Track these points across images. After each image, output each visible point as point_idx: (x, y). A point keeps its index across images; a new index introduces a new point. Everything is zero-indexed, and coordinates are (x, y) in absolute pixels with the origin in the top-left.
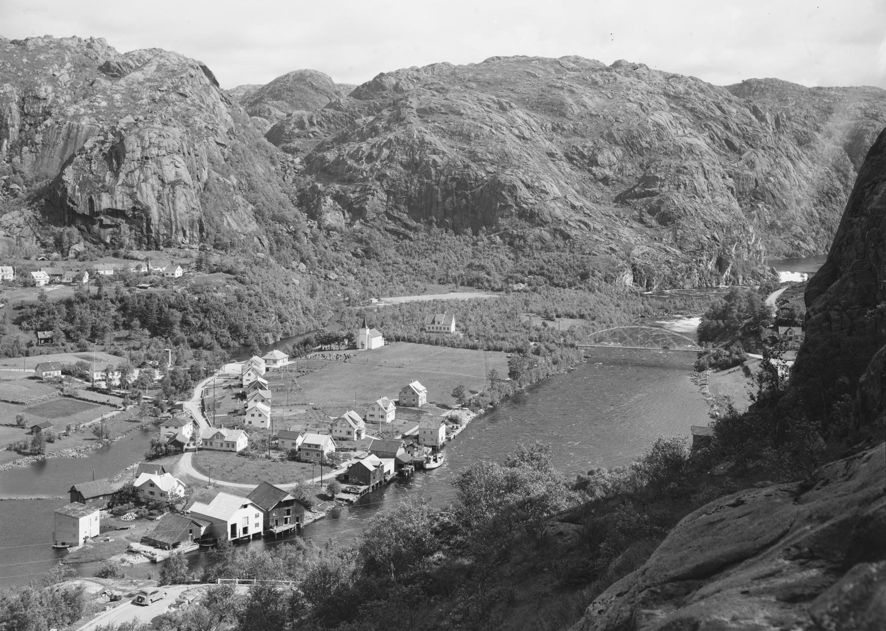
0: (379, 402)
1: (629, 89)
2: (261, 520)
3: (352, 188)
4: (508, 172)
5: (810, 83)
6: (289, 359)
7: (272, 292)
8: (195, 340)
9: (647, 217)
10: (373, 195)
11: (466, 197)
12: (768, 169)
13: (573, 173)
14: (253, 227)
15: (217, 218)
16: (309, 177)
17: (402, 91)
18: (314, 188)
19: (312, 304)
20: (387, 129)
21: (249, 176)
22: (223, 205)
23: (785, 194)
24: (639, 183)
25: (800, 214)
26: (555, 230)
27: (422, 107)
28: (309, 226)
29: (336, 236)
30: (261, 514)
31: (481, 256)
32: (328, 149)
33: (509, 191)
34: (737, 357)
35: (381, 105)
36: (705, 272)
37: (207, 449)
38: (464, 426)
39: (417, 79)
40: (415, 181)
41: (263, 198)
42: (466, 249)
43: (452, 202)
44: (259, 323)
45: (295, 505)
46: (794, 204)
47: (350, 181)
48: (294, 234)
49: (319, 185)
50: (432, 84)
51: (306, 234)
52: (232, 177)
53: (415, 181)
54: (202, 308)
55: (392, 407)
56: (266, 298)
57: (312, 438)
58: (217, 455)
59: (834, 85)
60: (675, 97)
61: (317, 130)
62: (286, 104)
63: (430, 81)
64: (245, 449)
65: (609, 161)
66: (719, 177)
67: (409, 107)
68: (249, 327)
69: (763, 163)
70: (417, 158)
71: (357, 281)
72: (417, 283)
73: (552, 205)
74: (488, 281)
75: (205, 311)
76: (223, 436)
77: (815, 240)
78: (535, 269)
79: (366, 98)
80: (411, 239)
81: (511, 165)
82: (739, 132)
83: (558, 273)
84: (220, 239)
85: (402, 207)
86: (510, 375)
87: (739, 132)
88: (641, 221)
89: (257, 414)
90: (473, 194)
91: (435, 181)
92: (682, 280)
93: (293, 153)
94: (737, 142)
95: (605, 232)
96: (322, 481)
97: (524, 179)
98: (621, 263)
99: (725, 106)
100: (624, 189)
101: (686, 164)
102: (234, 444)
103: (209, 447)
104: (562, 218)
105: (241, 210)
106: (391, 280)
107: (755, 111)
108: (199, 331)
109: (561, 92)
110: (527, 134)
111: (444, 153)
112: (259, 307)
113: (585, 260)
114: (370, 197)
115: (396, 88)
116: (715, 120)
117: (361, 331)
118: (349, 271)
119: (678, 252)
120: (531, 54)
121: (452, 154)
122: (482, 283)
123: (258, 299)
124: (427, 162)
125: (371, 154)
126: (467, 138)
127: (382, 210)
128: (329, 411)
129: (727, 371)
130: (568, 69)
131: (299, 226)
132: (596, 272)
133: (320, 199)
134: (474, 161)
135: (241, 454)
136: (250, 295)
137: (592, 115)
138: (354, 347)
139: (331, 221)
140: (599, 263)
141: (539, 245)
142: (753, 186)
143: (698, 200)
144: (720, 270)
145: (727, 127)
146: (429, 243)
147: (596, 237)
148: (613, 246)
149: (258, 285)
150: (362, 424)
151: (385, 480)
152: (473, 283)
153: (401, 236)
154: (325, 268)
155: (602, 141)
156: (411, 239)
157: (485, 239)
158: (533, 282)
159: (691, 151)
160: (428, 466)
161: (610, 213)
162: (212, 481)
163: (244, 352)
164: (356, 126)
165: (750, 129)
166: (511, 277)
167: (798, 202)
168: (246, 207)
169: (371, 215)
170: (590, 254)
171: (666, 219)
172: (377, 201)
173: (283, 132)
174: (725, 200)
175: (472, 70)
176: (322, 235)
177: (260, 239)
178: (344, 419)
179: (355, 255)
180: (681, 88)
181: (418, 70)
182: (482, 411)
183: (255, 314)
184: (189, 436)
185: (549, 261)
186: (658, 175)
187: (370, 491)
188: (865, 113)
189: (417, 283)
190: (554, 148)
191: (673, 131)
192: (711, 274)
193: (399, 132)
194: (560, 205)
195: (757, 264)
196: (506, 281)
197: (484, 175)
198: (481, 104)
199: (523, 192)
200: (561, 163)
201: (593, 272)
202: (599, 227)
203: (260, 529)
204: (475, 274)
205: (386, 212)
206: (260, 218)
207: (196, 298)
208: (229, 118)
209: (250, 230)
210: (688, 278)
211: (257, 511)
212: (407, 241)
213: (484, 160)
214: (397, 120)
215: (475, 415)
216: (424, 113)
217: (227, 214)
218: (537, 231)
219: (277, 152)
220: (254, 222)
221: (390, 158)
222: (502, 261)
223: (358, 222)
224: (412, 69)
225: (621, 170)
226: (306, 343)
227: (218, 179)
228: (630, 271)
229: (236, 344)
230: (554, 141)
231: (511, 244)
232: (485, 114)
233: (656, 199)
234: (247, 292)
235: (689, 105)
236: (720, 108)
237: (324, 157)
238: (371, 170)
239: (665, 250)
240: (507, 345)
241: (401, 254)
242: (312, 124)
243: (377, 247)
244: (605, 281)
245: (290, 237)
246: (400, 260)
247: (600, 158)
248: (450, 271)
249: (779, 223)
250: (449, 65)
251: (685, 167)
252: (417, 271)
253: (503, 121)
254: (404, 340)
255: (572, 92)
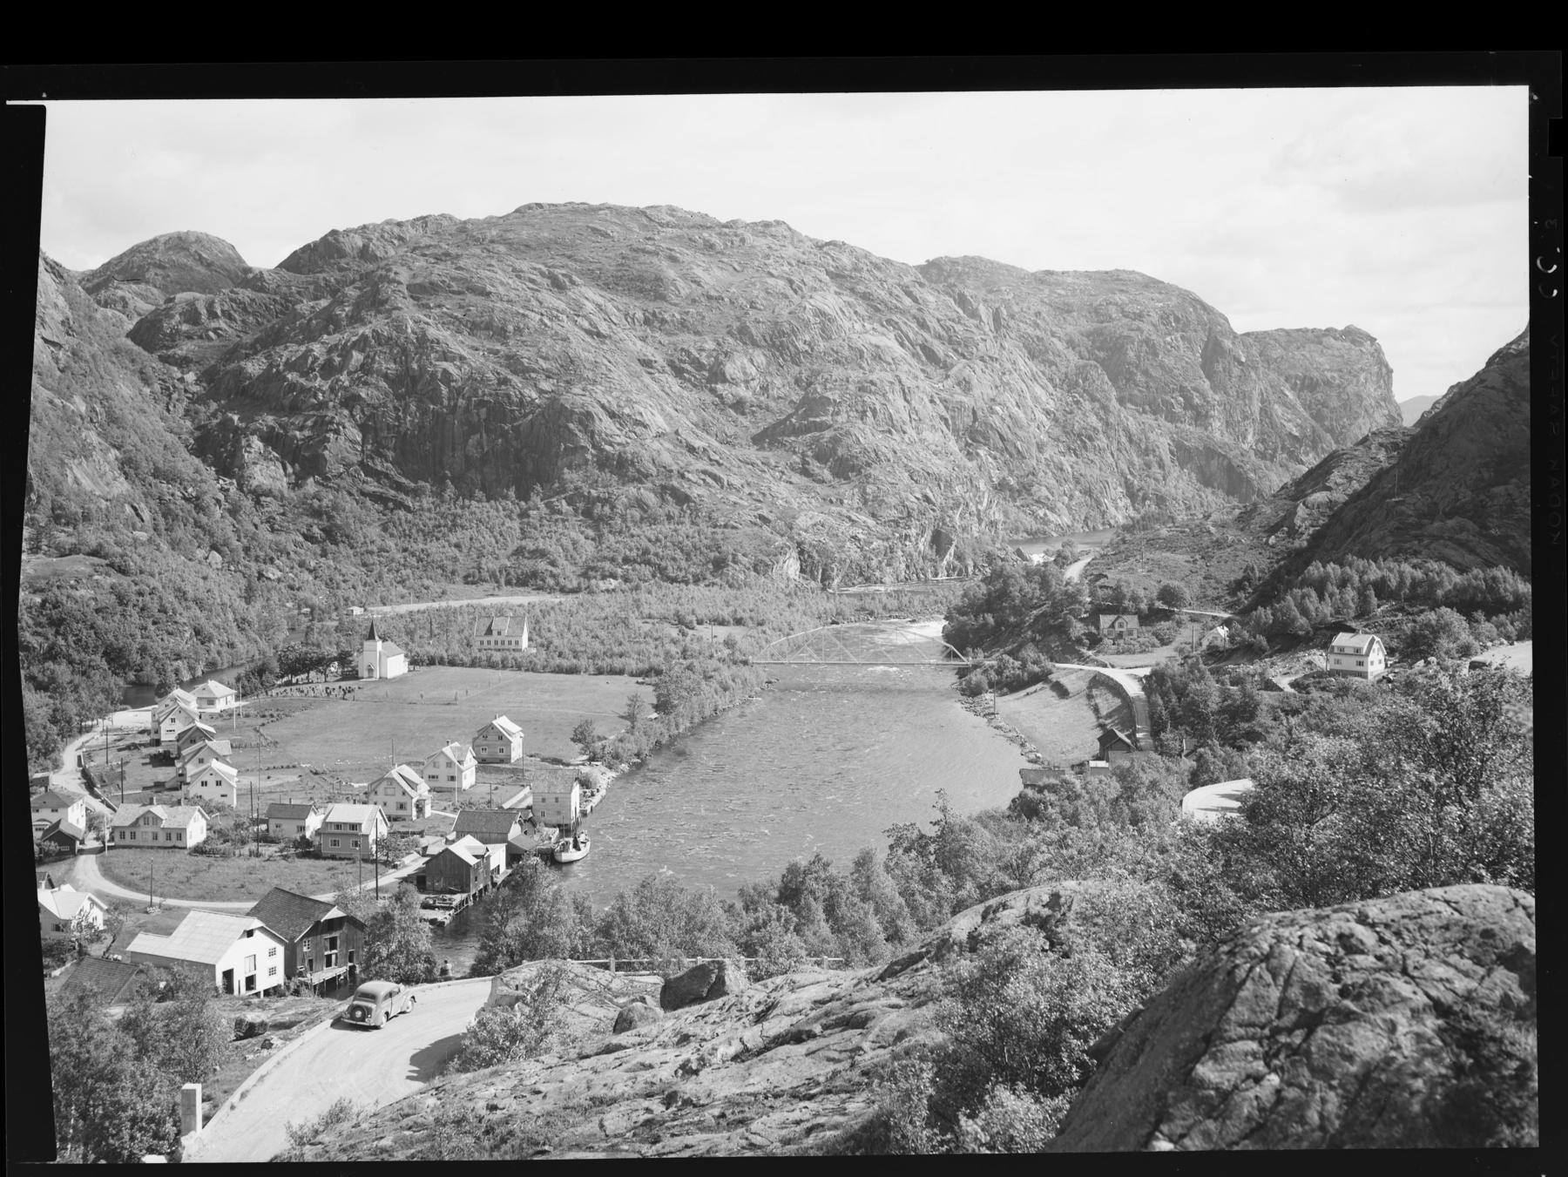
0: (447, 750)
1: (767, 257)
2: (279, 961)
3: (298, 421)
4: (577, 390)
5: (1033, 265)
6: (237, 698)
7: (179, 590)
8: (40, 677)
9: (815, 466)
10: (337, 432)
11: (504, 434)
12: (992, 393)
13: (685, 393)
14: (122, 486)
15: (54, 471)
16: (214, 406)
17: (375, 258)
18: (226, 424)
19: (253, 612)
20: (355, 319)
21: (107, 398)
22: (63, 446)
23: (1020, 433)
24: (797, 410)
25: (1043, 467)
26: (664, 488)
27: (418, 281)
28: (222, 489)
29: (273, 506)
30: (281, 949)
31: (536, 534)
32: (247, 356)
33: (581, 422)
34: (1036, 669)
35: (338, 282)
36: (915, 555)
37: (124, 847)
38: (603, 792)
39: (401, 238)
40: (413, 408)
41: (136, 439)
42: (508, 523)
43: (480, 443)
44: (161, 644)
45: (345, 929)
46: (1034, 449)
47: (294, 409)
48: (197, 502)
49: (236, 418)
50: (428, 247)
51: (218, 501)
52: (77, 399)
53: (413, 408)
54: (50, 618)
55: (470, 762)
56: (170, 598)
57: (343, 812)
58: (151, 856)
59: (1070, 269)
60: (838, 276)
61: (223, 326)
62: (155, 291)
63: (425, 241)
64: (205, 842)
65: (745, 373)
66: (926, 400)
67: (394, 281)
68: (143, 650)
69: (983, 386)
70: (415, 366)
71: (318, 582)
72: (427, 582)
73: (656, 445)
74: (553, 576)
75: (57, 623)
76: (157, 819)
77: (1069, 508)
78: (634, 554)
79: (309, 271)
80: (408, 509)
81: (582, 379)
82: (943, 333)
83: (674, 559)
84: (61, 507)
85: (390, 454)
86: (657, 708)
87: (943, 333)
88: (805, 472)
89: (211, 781)
90: (516, 429)
91: (448, 407)
92: (879, 568)
93: (180, 366)
94: (940, 349)
95: (747, 490)
96: (377, 889)
97: (604, 401)
98: (780, 541)
99: (916, 291)
100: (771, 420)
101: (873, 377)
102: (181, 834)
103: (128, 841)
104: (675, 467)
105: (97, 456)
106: (380, 577)
107: (962, 301)
108: (45, 660)
109: (655, 260)
110: (603, 328)
111: (462, 358)
112: (157, 615)
113: (719, 537)
114: (331, 435)
115: (364, 253)
116: (903, 312)
117: (367, 644)
118: (302, 564)
119: (871, 522)
120: (595, 201)
121: (476, 360)
122: (543, 580)
123: (156, 600)
124: (433, 375)
125: (329, 362)
126: (501, 334)
127: (355, 459)
128: (345, 775)
129: (1023, 693)
130: (662, 225)
131: (205, 487)
132: (740, 556)
133: (239, 441)
134: (515, 372)
135: (199, 850)
136: (140, 594)
137: (710, 298)
138: (354, 675)
139: (261, 479)
140: (741, 541)
141: (637, 513)
142: (969, 421)
143: (896, 436)
144: (938, 552)
145: (923, 325)
146: (443, 516)
147: (733, 498)
148: (765, 513)
149: (152, 575)
150: (424, 788)
151: (494, 884)
152: (526, 580)
153: (391, 505)
154: (257, 559)
155: (731, 340)
156: (408, 509)
157: (541, 505)
158: (633, 575)
159: (878, 357)
160: (565, 857)
161: (754, 459)
162: (156, 900)
163: (143, 691)
164: (297, 316)
165: (958, 328)
166: (592, 569)
167: (1040, 447)
168: (105, 452)
169: (334, 468)
170: (726, 526)
171: (845, 468)
172: (345, 442)
173: (160, 329)
174: (938, 437)
175: (495, 225)
176: (248, 503)
177: (135, 509)
178: (392, 780)
179: (309, 538)
180: (846, 260)
181: (399, 224)
182: (624, 767)
183: (152, 628)
184: (82, 825)
185: (658, 540)
186: (828, 394)
187: (471, 903)
188: (1123, 312)
189: (427, 582)
190: (649, 352)
191: (847, 324)
192: (924, 558)
193: (377, 323)
194: (667, 445)
195: (994, 542)
196: (585, 575)
197: (534, 395)
198: (519, 277)
199: (605, 425)
200: (663, 377)
201: (734, 556)
202: (736, 481)
203: (279, 979)
204: (528, 565)
205: (361, 463)
206: (132, 472)
207: (38, 600)
208: (61, 301)
209: (116, 492)
210: (889, 565)
211: (272, 944)
212: (402, 513)
213: (534, 371)
214: (373, 304)
215: (614, 774)
216: (421, 291)
217: (73, 463)
218: (632, 490)
219: (152, 362)
220: (122, 479)
221: (365, 368)
222: (574, 543)
223: (311, 480)
224: (387, 223)
225: (764, 389)
226: (261, 671)
227: (51, 402)
228: (795, 555)
229: (121, 682)
230: (650, 340)
231: (587, 513)
232: (529, 293)
233: (828, 434)
234: (135, 588)
235: (861, 288)
236: (909, 294)
237: (241, 370)
238: (332, 389)
239: (850, 518)
240: (632, 664)
241: (392, 535)
242: (213, 315)
243: (348, 524)
244: (756, 570)
245: (190, 507)
246: (391, 543)
247: (730, 369)
248: (484, 561)
249: (1012, 482)
250: (451, 218)
251: (872, 382)
252: (424, 561)
253: (563, 306)
254: (442, 662)
255: (673, 259)
